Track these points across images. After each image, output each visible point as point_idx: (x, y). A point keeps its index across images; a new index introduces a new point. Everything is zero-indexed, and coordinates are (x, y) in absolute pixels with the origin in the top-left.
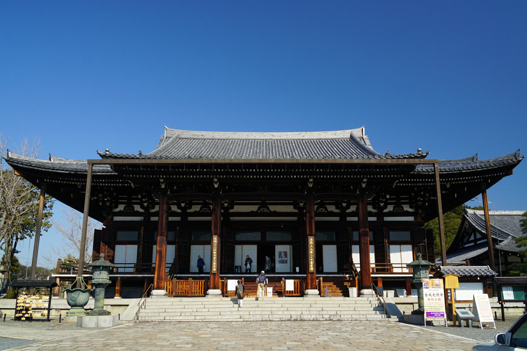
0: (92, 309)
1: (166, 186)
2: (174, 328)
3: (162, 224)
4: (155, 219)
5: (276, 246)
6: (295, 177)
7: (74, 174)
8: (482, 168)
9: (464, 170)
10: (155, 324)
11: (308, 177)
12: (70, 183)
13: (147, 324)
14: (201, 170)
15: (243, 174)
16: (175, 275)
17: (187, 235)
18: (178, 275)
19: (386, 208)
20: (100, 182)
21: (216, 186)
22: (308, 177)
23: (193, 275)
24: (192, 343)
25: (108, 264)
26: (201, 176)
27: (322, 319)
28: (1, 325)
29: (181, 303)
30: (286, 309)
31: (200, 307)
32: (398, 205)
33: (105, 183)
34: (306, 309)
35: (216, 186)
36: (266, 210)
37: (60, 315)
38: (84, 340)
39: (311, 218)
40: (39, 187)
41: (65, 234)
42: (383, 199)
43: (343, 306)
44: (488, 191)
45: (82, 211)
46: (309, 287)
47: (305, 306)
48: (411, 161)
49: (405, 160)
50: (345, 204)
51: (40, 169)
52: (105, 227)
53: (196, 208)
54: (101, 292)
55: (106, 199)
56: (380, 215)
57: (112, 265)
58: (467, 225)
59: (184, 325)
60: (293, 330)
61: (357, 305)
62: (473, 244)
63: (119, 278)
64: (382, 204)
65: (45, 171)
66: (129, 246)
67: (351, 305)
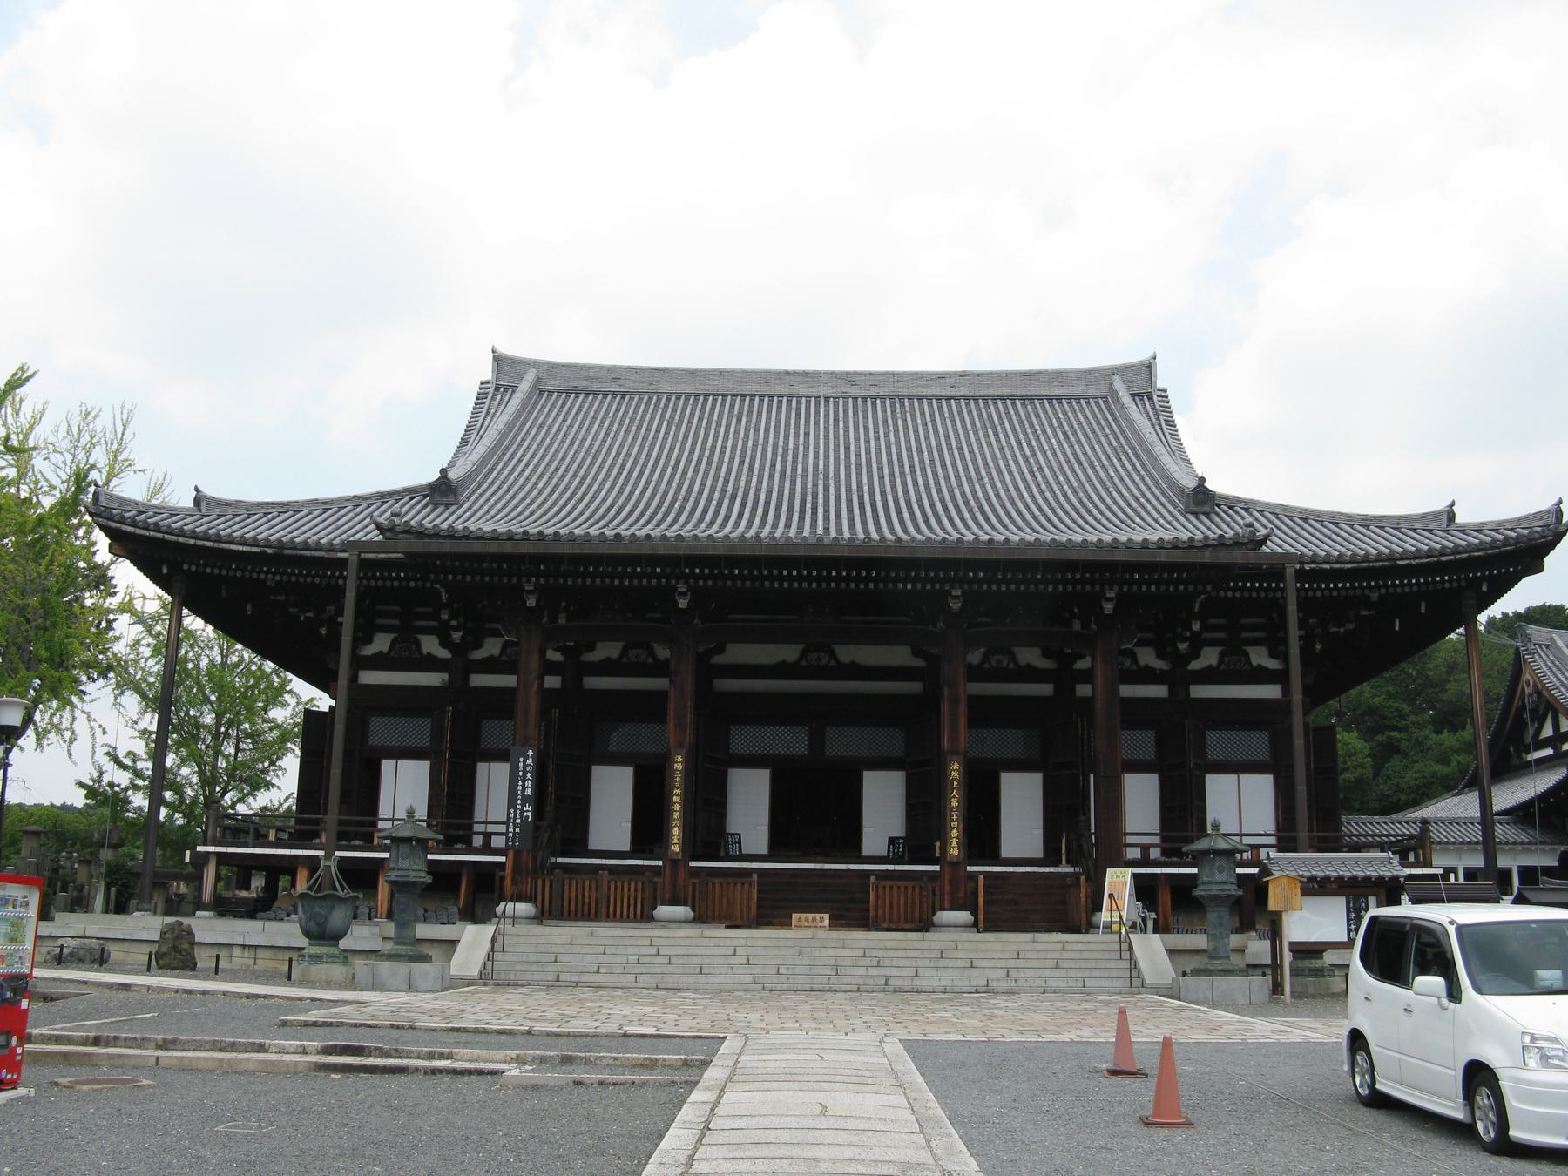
1: (538, 601)
5: (866, 774)
7: (275, 554)
19: (1197, 656)
21: (683, 603)
29: (593, 941)
32: (1234, 647)
34: (927, 963)
35: (683, 603)
43: (1028, 955)
47: (927, 954)
51: (181, 539)
56: (1178, 678)
61: (1066, 955)
62: (1549, 752)
64: (1183, 647)
66: (1248, 780)
67: (1049, 955)
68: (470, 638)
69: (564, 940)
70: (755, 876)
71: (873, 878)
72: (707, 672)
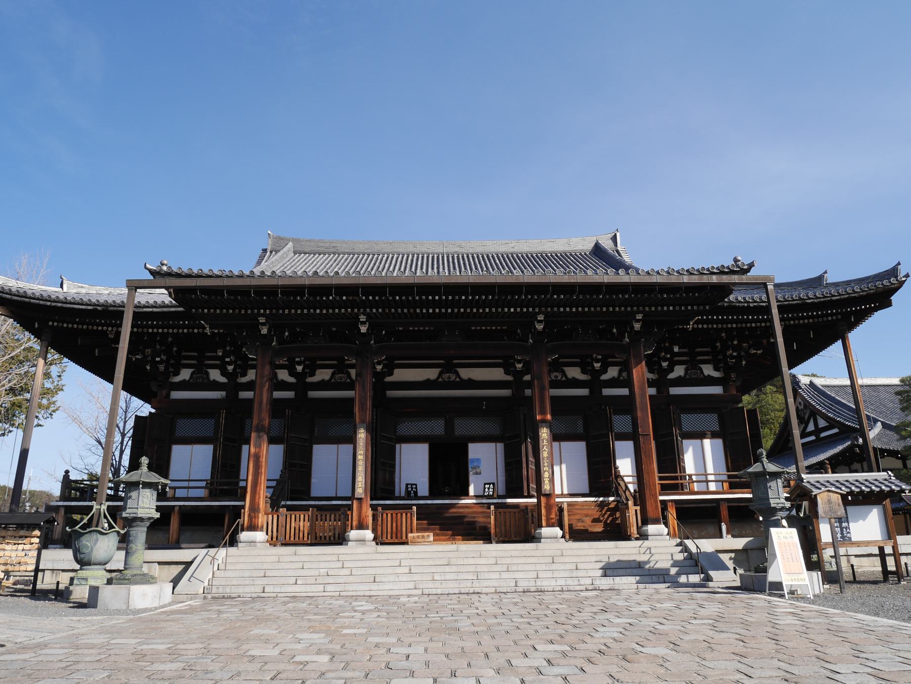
0: (120, 571)
2: (285, 611)
3: (261, 403)
4: (248, 395)
6: (512, 310)
7: (103, 311)
8: (840, 295)
9: (810, 299)
10: (244, 603)
11: (537, 310)
12: (95, 328)
13: (228, 602)
14: (338, 298)
15: (415, 304)
16: (283, 503)
17: (305, 426)
18: (289, 503)
20: (148, 327)
21: (363, 329)
22: (537, 310)
23: (317, 503)
24: (327, 652)
25: (154, 478)
26: (337, 311)
27: (578, 588)
30: (505, 568)
31: (333, 565)
32: (693, 365)
33: (158, 327)
34: (544, 567)
35: (363, 329)
36: (453, 377)
37: (58, 583)
38: (94, 641)
39: (542, 389)
40: (37, 334)
41: (78, 424)
42: (666, 353)
44: (853, 336)
45: (110, 378)
46: (544, 523)
47: (542, 560)
48: (725, 279)
49: (714, 277)
50: (599, 365)
52: (153, 411)
53: (323, 375)
54: (140, 534)
55: (158, 359)
57: (163, 480)
59: (304, 605)
60: (532, 612)
62: (813, 438)
64: (665, 364)
68: (307, 370)
69: (275, 559)
72: (380, 386)
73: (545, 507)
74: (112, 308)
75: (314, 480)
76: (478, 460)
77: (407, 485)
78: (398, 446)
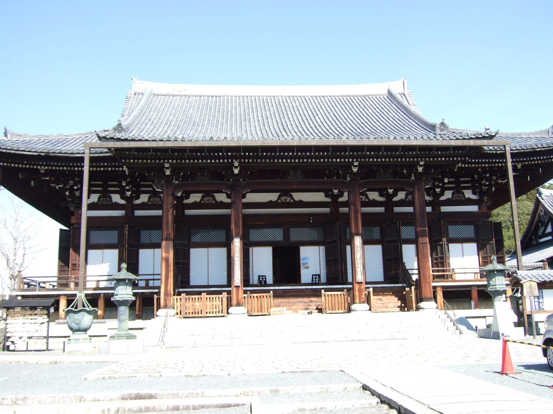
3: (168, 222)
9: (538, 148)
17: (187, 236)
21: (236, 171)
25: (132, 276)
28: (1, 354)
32: (458, 190)
35: (236, 171)
36: (288, 199)
42: (439, 183)
46: (357, 301)
50: (392, 190)
53: (195, 198)
54: (124, 311)
58: (541, 211)
63: (102, 296)
64: (438, 190)
65: (6, 153)
68: (134, 195)
70: (271, 292)
71: (323, 291)
73: (358, 291)
74: (52, 154)
75: (192, 274)
76: (306, 258)
77: (259, 276)
78: (251, 249)
